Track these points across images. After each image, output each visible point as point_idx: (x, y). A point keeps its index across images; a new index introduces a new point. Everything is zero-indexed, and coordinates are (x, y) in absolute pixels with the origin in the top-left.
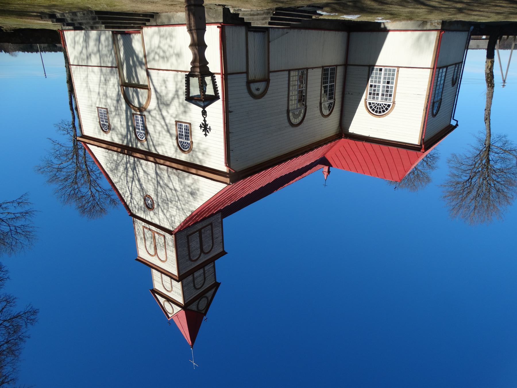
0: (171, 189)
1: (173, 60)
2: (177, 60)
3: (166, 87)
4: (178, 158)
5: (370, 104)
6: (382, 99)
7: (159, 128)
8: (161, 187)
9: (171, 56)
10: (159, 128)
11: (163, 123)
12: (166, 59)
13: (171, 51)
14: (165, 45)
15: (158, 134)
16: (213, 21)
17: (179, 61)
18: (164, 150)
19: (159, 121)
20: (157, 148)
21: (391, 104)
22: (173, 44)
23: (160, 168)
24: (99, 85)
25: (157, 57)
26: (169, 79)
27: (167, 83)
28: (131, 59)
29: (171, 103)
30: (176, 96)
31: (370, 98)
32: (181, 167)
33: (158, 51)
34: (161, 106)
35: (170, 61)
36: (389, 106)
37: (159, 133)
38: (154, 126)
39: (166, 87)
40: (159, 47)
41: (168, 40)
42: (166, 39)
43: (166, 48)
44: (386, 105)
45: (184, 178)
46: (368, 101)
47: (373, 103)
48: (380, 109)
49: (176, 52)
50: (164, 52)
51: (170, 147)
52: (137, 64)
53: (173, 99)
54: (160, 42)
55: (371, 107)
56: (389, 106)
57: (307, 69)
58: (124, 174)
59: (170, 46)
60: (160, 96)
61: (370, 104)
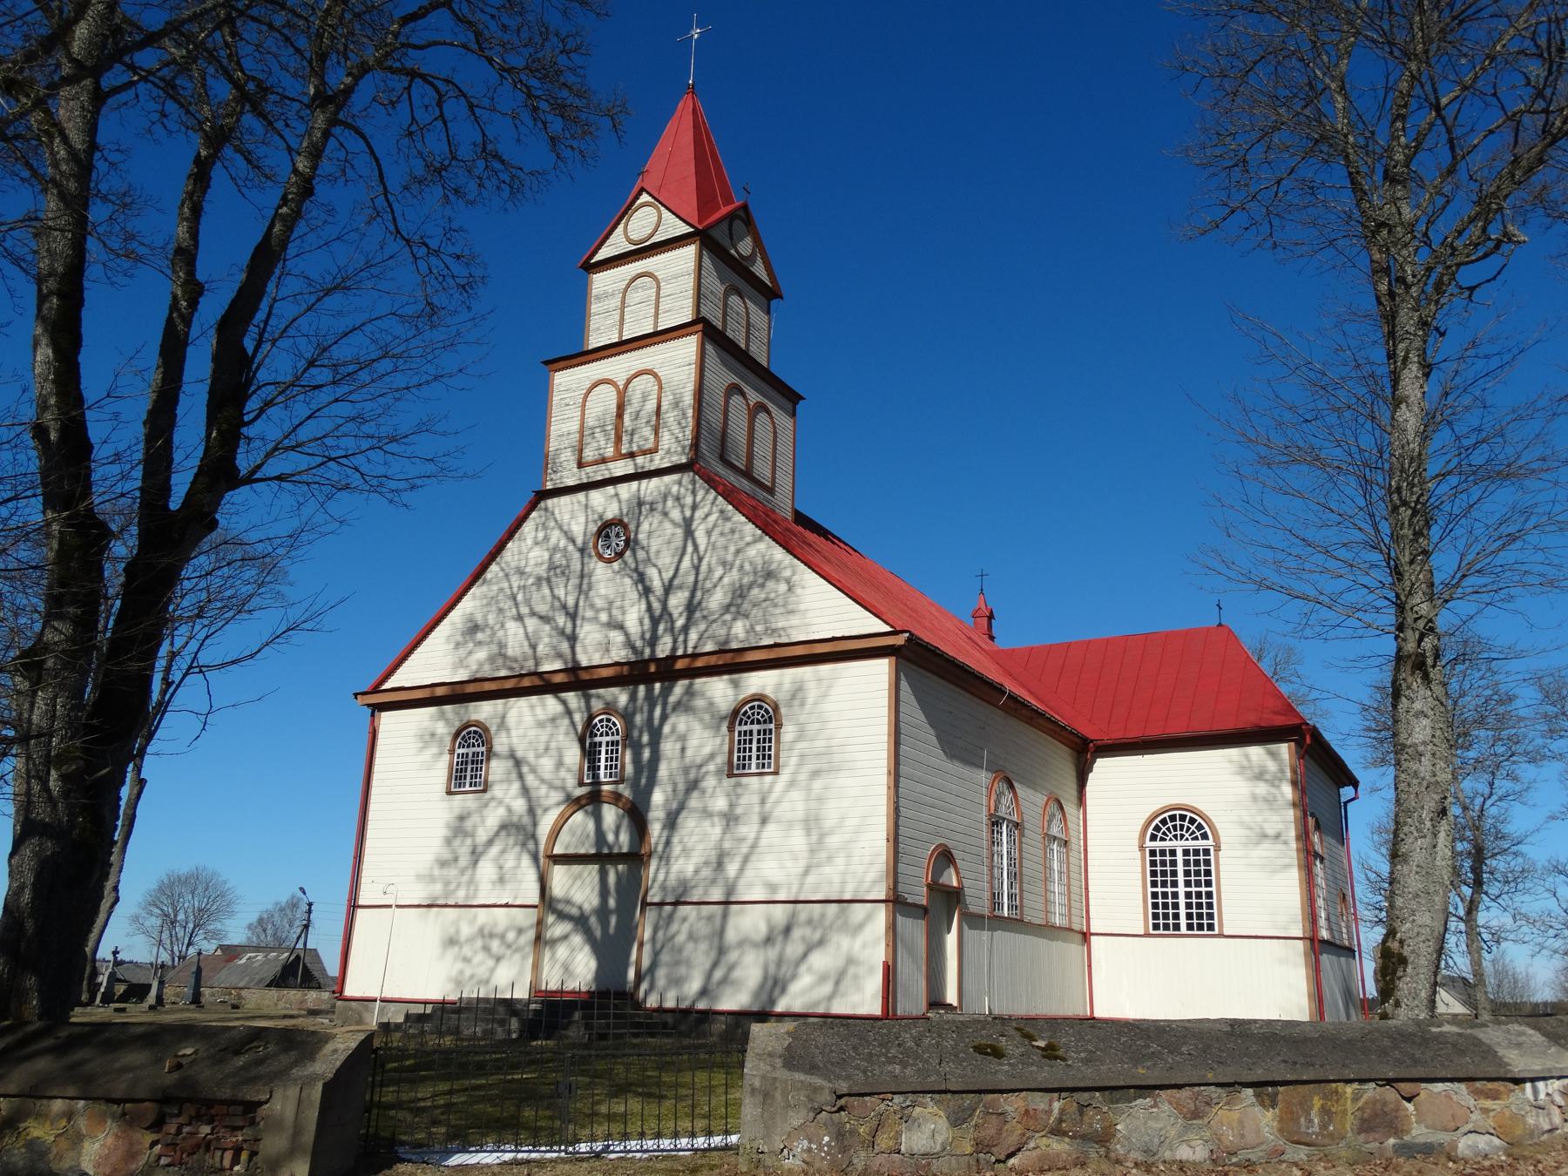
0: (533, 614)
1: (466, 930)
2: (458, 932)
3: (501, 868)
4: (499, 701)
5: (1205, 836)
6: (1173, 853)
7: (546, 764)
8: (564, 607)
9: (470, 940)
10: (546, 764)
11: (530, 780)
12: (486, 932)
13: (467, 951)
14: (479, 964)
15: (553, 745)
16: (354, 1004)
17: (452, 931)
18: (539, 711)
19: (543, 781)
20: (559, 708)
21: (1149, 844)
22: (459, 965)
23: (560, 655)
24: (754, 846)
25: (511, 936)
26: (490, 886)
27: (495, 877)
28: (612, 930)
29: (497, 834)
30: (480, 849)
31: (1207, 852)
32: (471, 689)
33: (502, 950)
34: (526, 820)
35: (475, 928)
36: (1153, 838)
37: (547, 749)
38: (560, 764)
39: (501, 868)
40: (498, 959)
41: (468, 973)
42: (472, 976)
43: (480, 956)
44: (1162, 839)
45: (491, 659)
46: (1210, 842)
47: (1196, 838)
48: (1175, 827)
49: (456, 949)
50: (486, 949)
51: (519, 722)
52: (593, 920)
53: (490, 842)
54: (492, 971)
55: (1200, 827)
56: (1153, 838)
57: (1147, 935)
58: (708, 585)
59: (466, 960)
60: (524, 845)
61: (1205, 836)
